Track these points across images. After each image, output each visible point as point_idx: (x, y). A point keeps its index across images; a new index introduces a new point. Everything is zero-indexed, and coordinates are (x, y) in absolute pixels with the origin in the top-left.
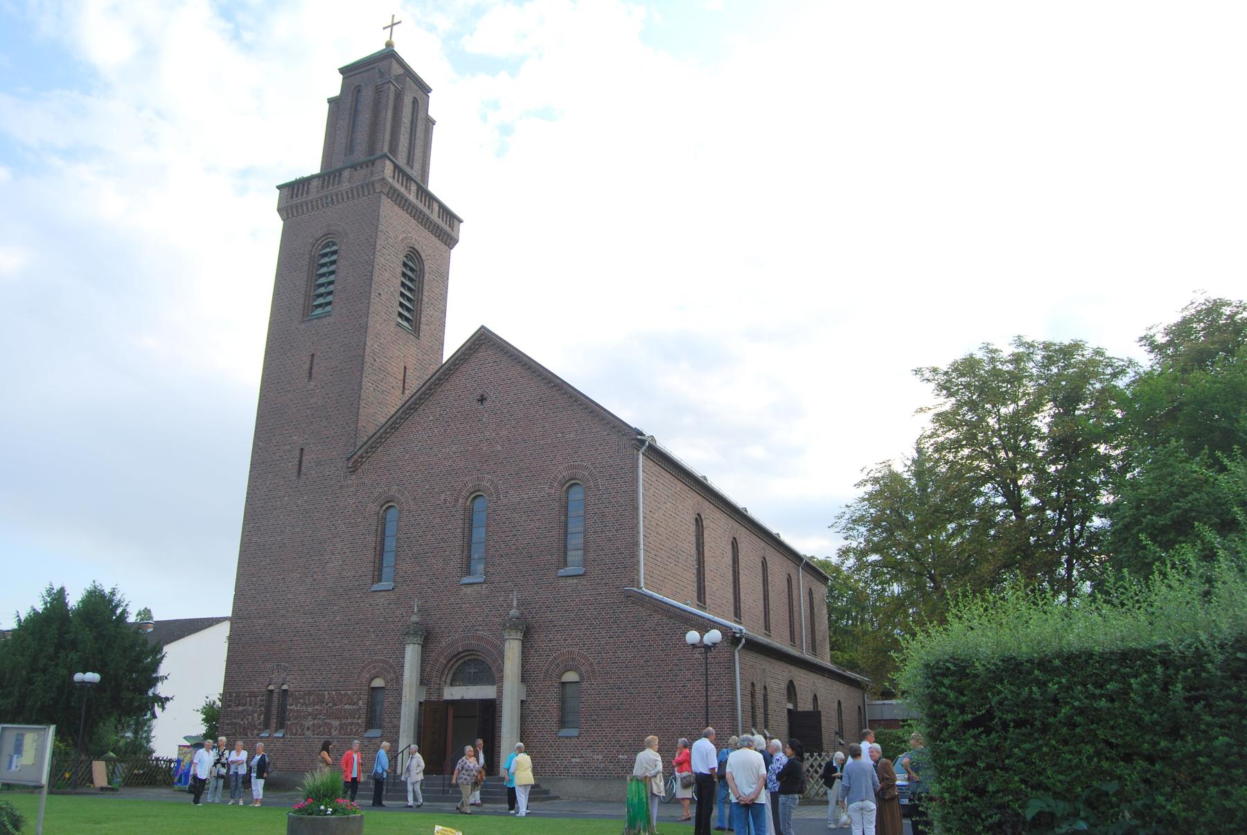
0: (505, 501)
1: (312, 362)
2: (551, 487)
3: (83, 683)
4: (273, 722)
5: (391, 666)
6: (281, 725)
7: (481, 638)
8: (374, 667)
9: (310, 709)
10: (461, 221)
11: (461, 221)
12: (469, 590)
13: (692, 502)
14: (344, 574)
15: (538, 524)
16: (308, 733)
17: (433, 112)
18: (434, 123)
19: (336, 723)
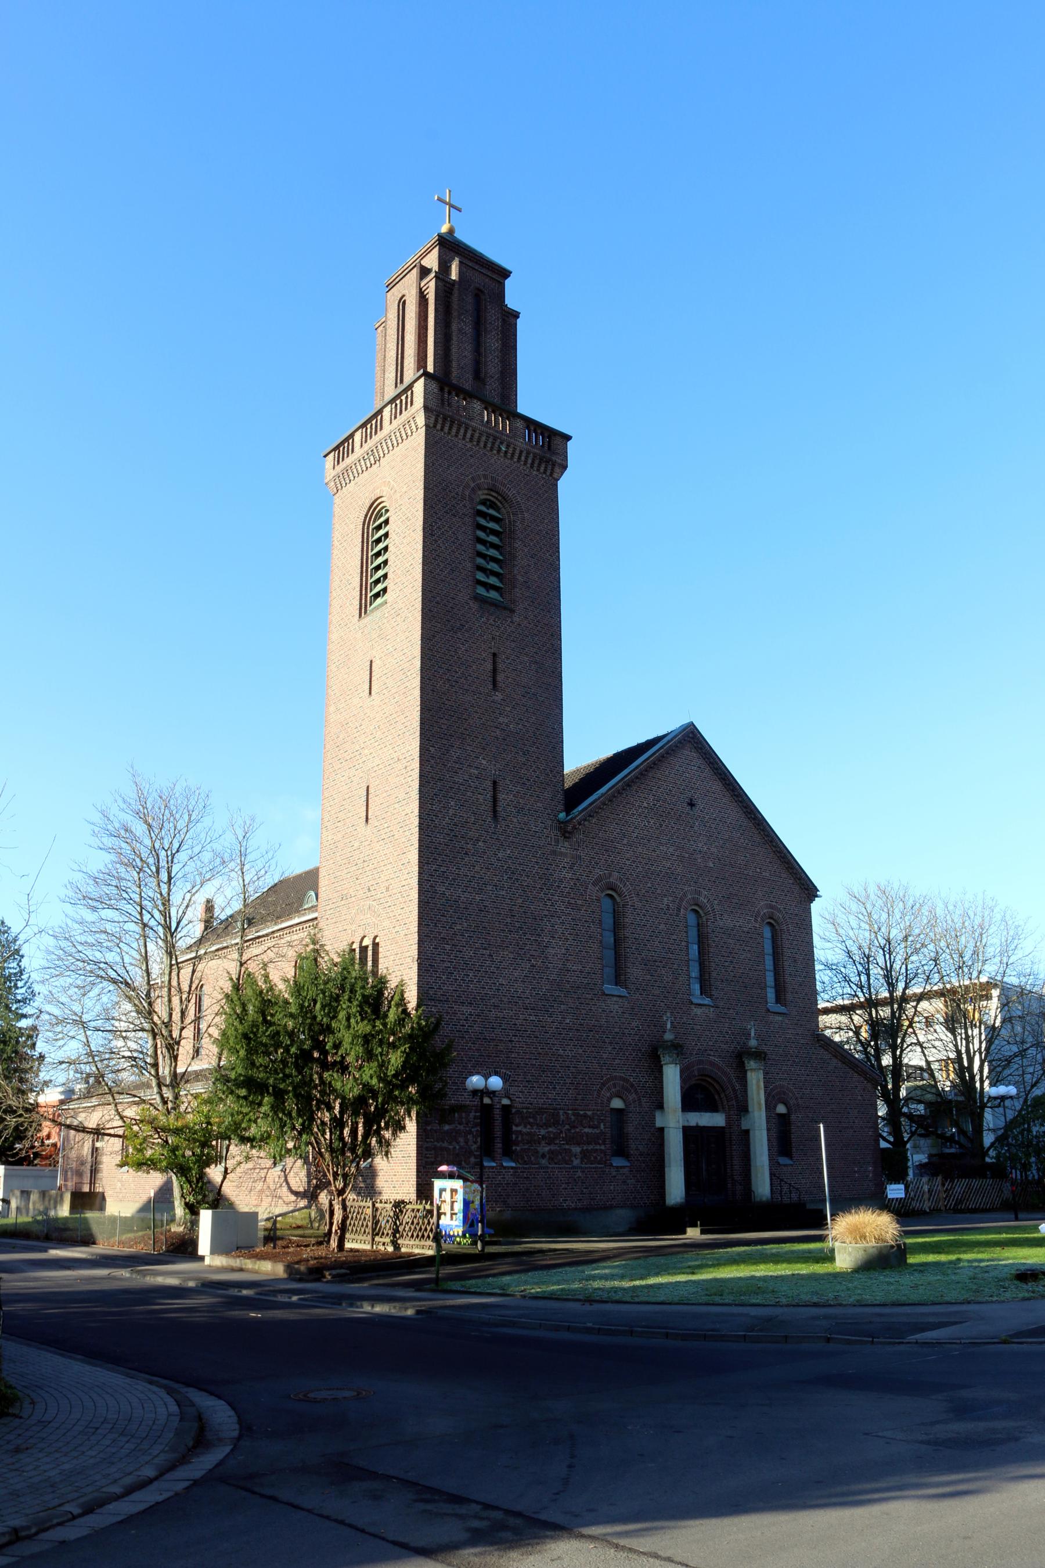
0: (721, 923)
1: (494, 663)
2: (756, 921)
3: (461, 273)
4: (499, 1146)
5: (632, 1086)
6: (508, 1153)
7: (712, 1064)
8: (615, 1085)
9: (543, 1132)
10: (568, 438)
11: (568, 438)
12: (698, 1011)
13: (734, 814)
14: (569, 965)
15: (749, 956)
16: (544, 1162)
17: (511, 301)
18: (516, 315)
19: (576, 1149)
